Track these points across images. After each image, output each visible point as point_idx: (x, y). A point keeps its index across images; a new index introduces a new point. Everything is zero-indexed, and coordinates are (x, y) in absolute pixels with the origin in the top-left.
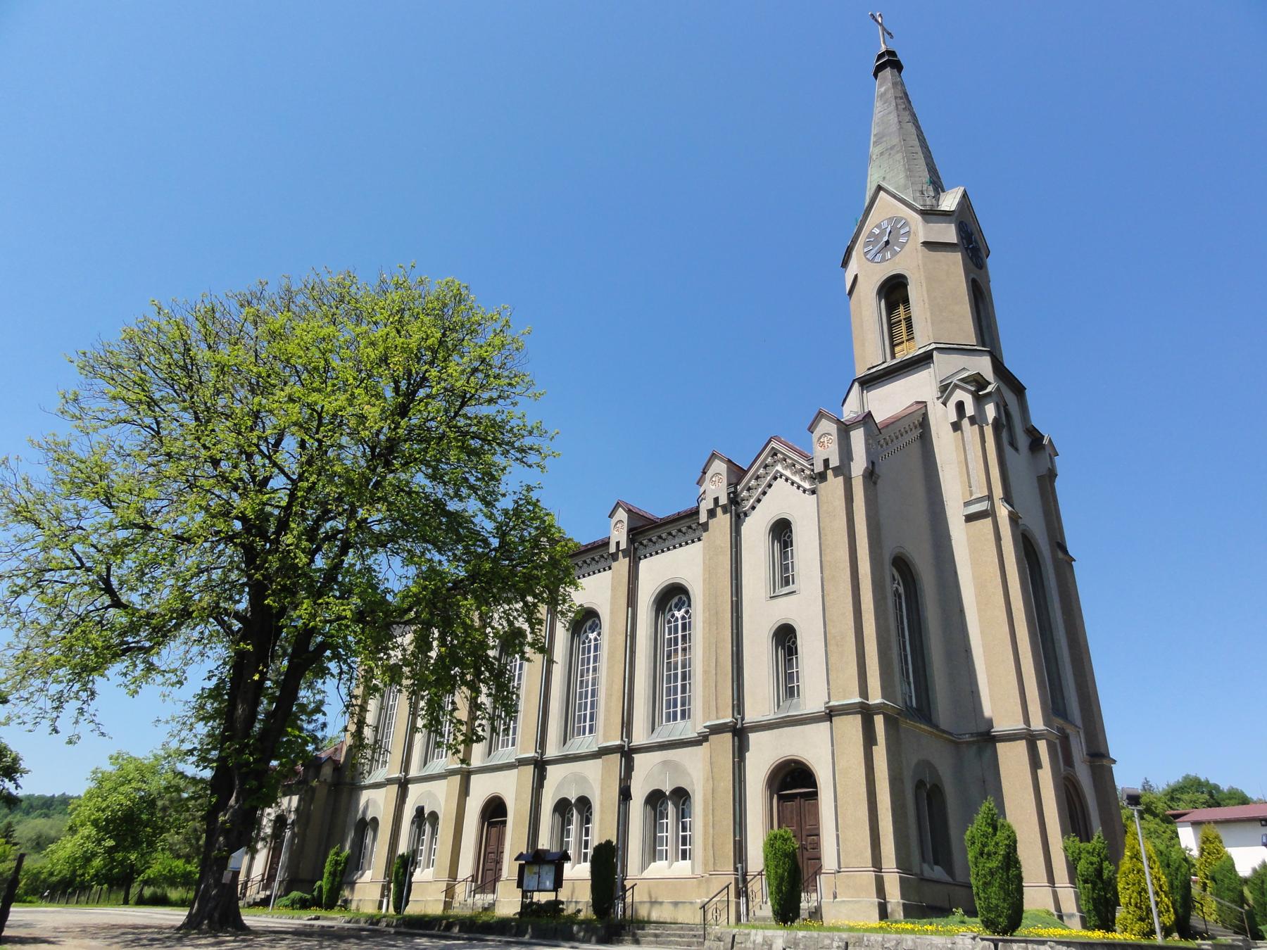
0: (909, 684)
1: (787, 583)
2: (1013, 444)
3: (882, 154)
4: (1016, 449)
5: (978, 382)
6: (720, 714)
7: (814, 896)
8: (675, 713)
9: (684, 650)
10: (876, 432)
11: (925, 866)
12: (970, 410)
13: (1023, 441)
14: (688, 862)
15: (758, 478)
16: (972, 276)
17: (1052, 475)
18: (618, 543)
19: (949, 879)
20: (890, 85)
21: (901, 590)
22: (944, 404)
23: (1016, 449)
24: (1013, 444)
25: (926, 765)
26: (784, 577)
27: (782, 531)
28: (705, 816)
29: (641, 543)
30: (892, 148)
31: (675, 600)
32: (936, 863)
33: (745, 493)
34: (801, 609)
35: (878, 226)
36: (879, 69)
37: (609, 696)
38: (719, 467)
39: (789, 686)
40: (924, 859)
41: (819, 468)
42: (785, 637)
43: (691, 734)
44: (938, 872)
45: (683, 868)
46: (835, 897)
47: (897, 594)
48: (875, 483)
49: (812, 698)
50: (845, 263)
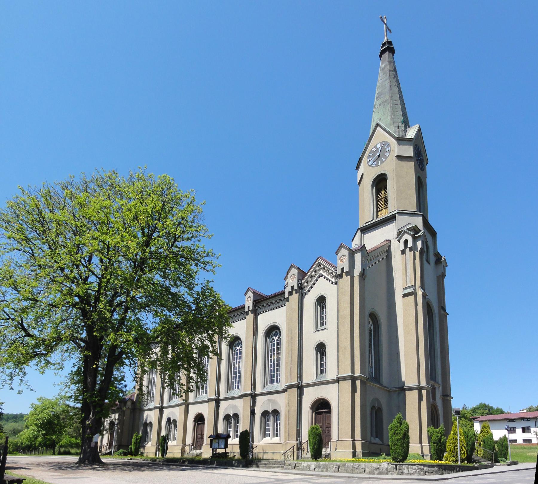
0: (372, 368)
1: (323, 325)
2: (428, 261)
3: (380, 105)
4: (429, 263)
5: (415, 230)
6: (292, 381)
7: (328, 449)
8: (274, 380)
9: (278, 354)
10: (367, 255)
11: (372, 438)
12: (410, 244)
13: (432, 259)
14: (278, 438)
15: (312, 277)
16: (418, 175)
17: (444, 275)
18: (249, 307)
19: (381, 443)
20: (387, 63)
21: (372, 328)
22: (399, 241)
23: (429, 263)
24: (428, 261)
25: (377, 400)
26: (321, 322)
27: (321, 301)
28: (286, 420)
29: (259, 307)
30: (385, 102)
31: (274, 332)
32: (377, 437)
33: (305, 284)
34: (328, 336)
35: (375, 147)
36: (383, 52)
37: (246, 373)
38: (294, 271)
39: (321, 369)
40: (372, 435)
41: (339, 272)
42: (321, 348)
43: (280, 388)
44: (377, 440)
45: (276, 440)
46: (336, 450)
47: (370, 329)
48: (364, 279)
49: (331, 374)
50: (358, 168)
